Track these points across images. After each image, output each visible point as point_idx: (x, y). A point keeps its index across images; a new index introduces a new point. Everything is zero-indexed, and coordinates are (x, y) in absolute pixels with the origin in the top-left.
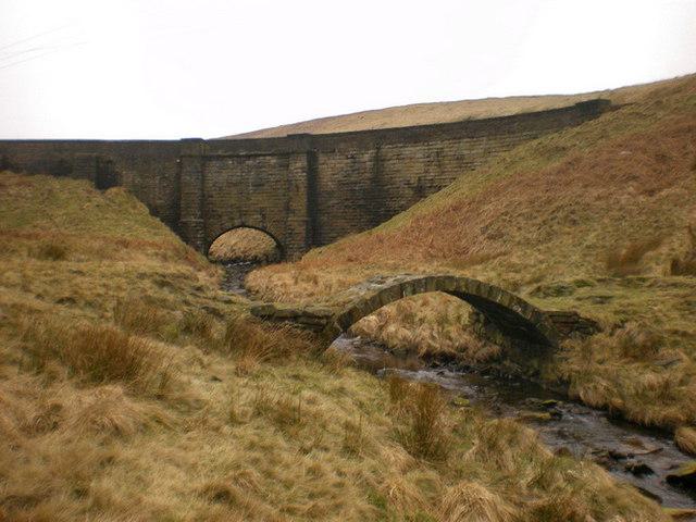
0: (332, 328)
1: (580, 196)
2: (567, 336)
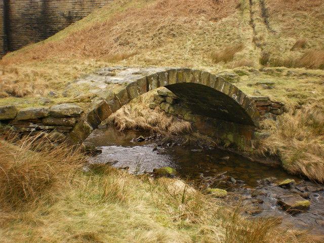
0: (81, 128)
1: (174, 21)
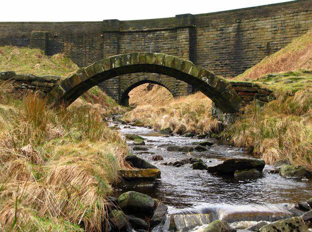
2: (248, 102)
